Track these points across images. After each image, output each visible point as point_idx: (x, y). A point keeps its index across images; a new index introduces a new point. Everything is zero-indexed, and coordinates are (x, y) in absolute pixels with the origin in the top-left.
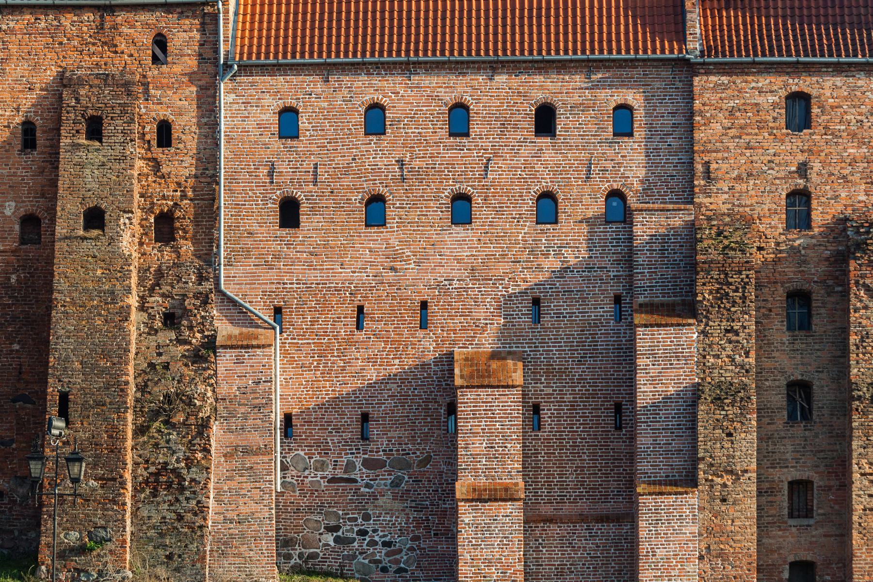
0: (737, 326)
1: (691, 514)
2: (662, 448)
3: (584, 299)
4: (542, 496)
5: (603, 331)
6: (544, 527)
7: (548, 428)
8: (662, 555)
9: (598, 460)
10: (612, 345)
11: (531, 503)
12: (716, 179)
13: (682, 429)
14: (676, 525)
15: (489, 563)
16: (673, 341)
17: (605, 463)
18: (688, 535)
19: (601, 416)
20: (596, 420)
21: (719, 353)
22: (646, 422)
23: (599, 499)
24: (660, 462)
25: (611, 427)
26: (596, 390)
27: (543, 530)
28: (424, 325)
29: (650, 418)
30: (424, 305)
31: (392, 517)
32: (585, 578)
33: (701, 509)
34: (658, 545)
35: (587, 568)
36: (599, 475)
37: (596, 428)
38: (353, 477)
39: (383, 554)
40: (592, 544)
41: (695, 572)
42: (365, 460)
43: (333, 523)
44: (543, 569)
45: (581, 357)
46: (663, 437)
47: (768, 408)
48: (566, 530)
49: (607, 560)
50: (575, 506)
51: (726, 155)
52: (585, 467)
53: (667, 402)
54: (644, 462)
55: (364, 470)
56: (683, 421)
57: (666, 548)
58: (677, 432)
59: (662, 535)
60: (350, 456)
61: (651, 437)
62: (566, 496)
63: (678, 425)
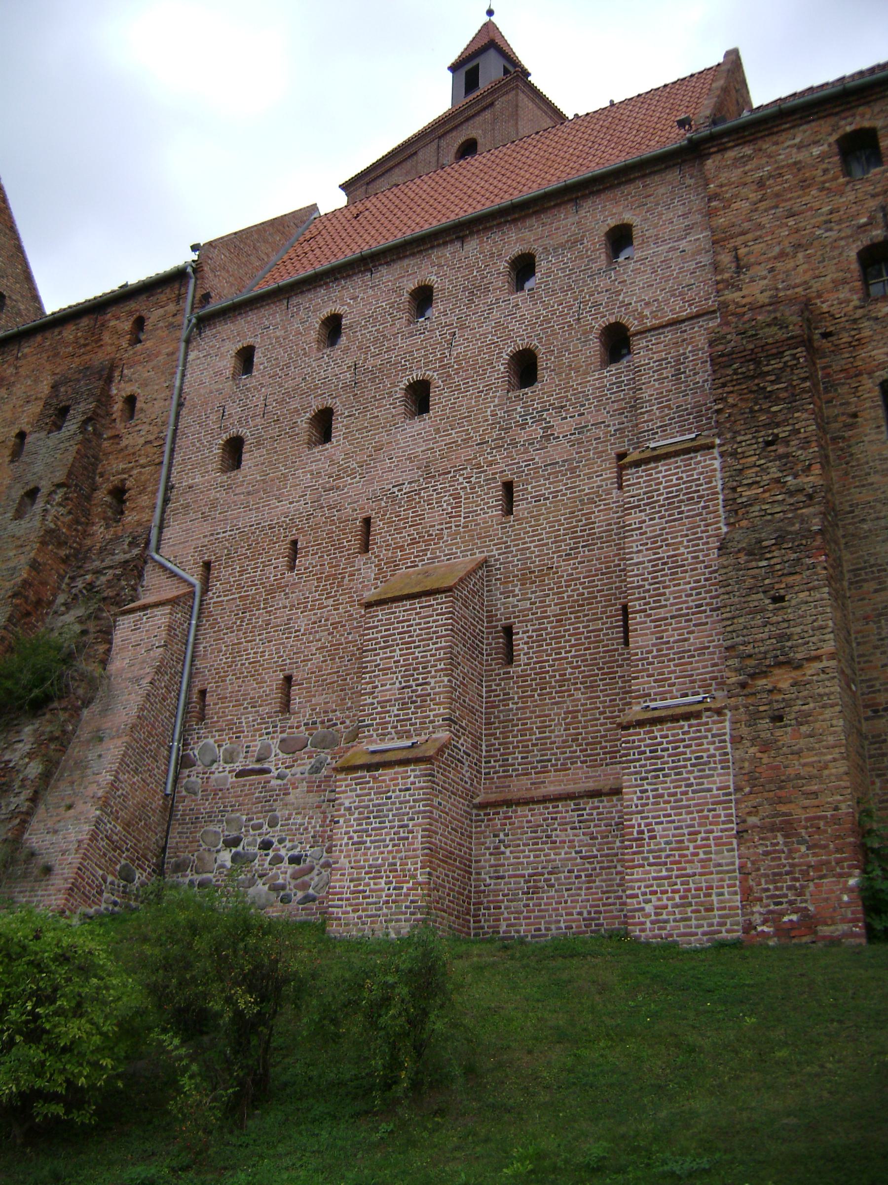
0: (782, 432)
1: (717, 753)
2: (672, 648)
3: (573, 470)
4: (513, 765)
5: (602, 507)
6: (507, 812)
7: (523, 659)
8: (667, 836)
9: (599, 697)
10: (615, 523)
11: (498, 778)
12: (748, 267)
13: (705, 611)
14: (691, 776)
15: (376, 871)
16: (681, 478)
17: (611, 701)
18: (715, 792)
19: (602, 630)
20: (595, 636)
21: (758, 479)
22: (645, 611)
23: (601, 760)
24: (669, 673)
25: (618, 644)
26: (593, 592)
27: (505, 818)
28: (365, 547)
29: (649, 603)
30: (367, 521)
31: (304, 818)
32: (572, 895)
33: (737, 740)
34: (659, 817)
35: (577, 877)
36: (602, 721)
37: (595, 648)
38: (266, 766)
39: (288, 875)
40: (584, 834)
41: (733, 863)
42: (283, 741)
43: (234, 834)
44: (505, 884)
45: (571, 549)
46: (673, 630)
47: (871, 566)
48: (541, 814)
49: (608, 861)
50: (565, 775)
51: (758, 233)
52: (579, 711)
53: (677, 573)
54: (643, 677)
55: (281, 755)
56: (705, 599)
57: (673, 822)
58: (697, 619)
59: (666, 798)
60: (265, 737)
61: (652, 633)
62: (550, 760)
63: (697, 606)
